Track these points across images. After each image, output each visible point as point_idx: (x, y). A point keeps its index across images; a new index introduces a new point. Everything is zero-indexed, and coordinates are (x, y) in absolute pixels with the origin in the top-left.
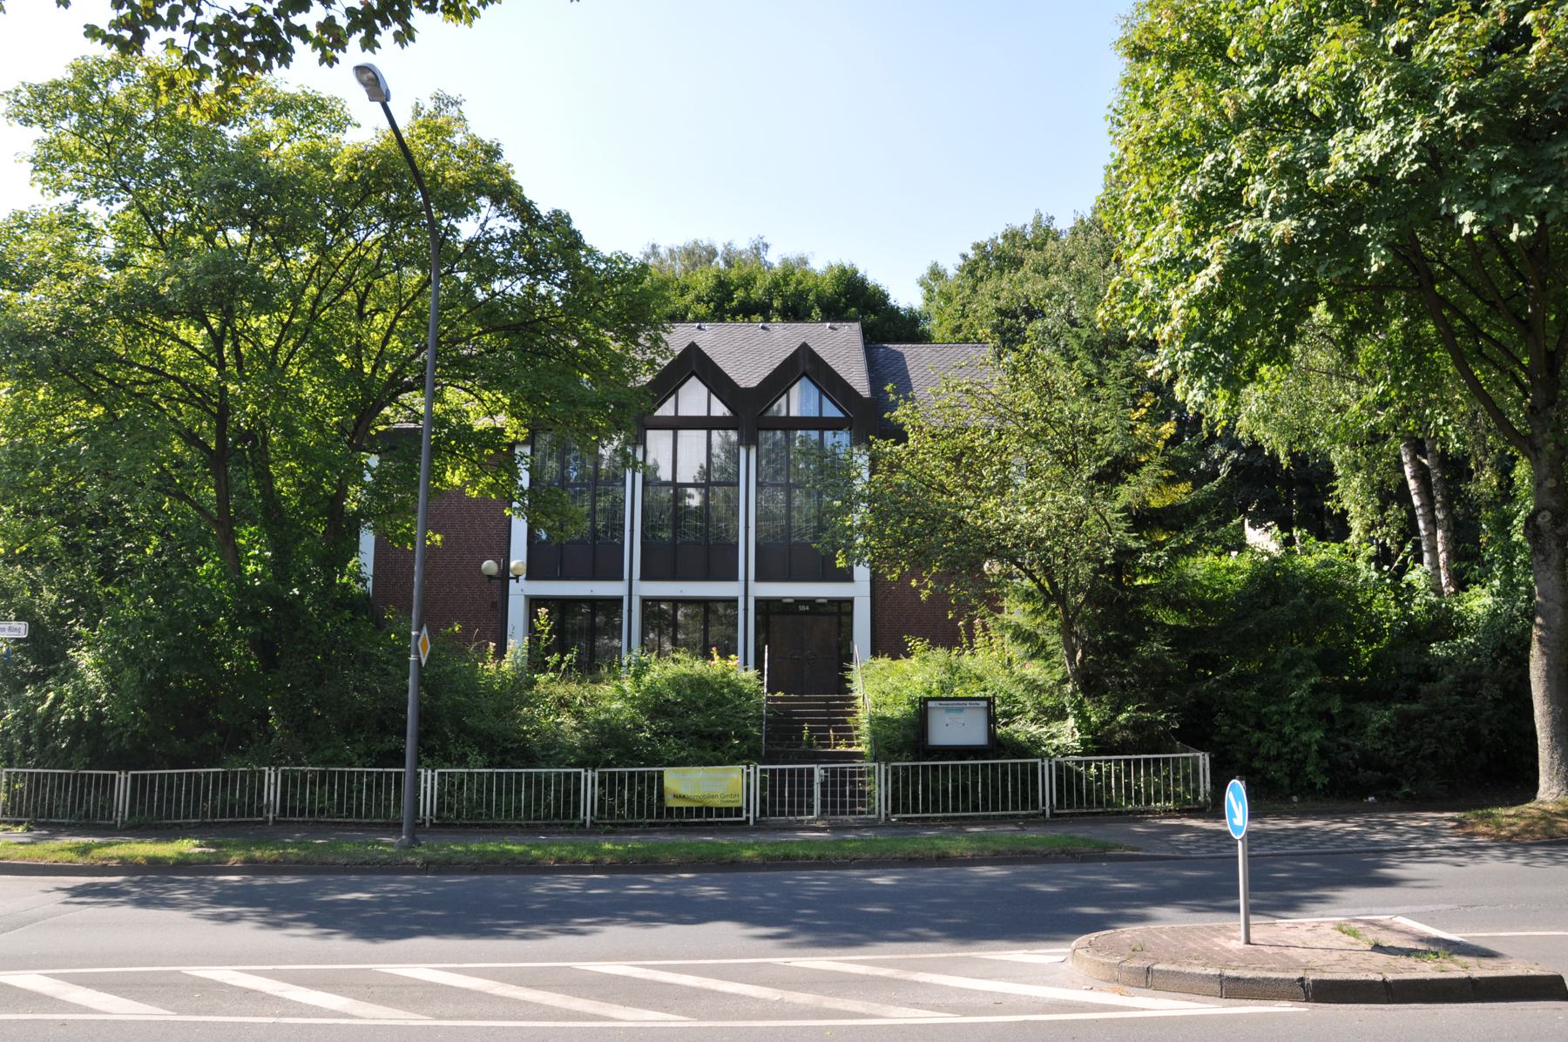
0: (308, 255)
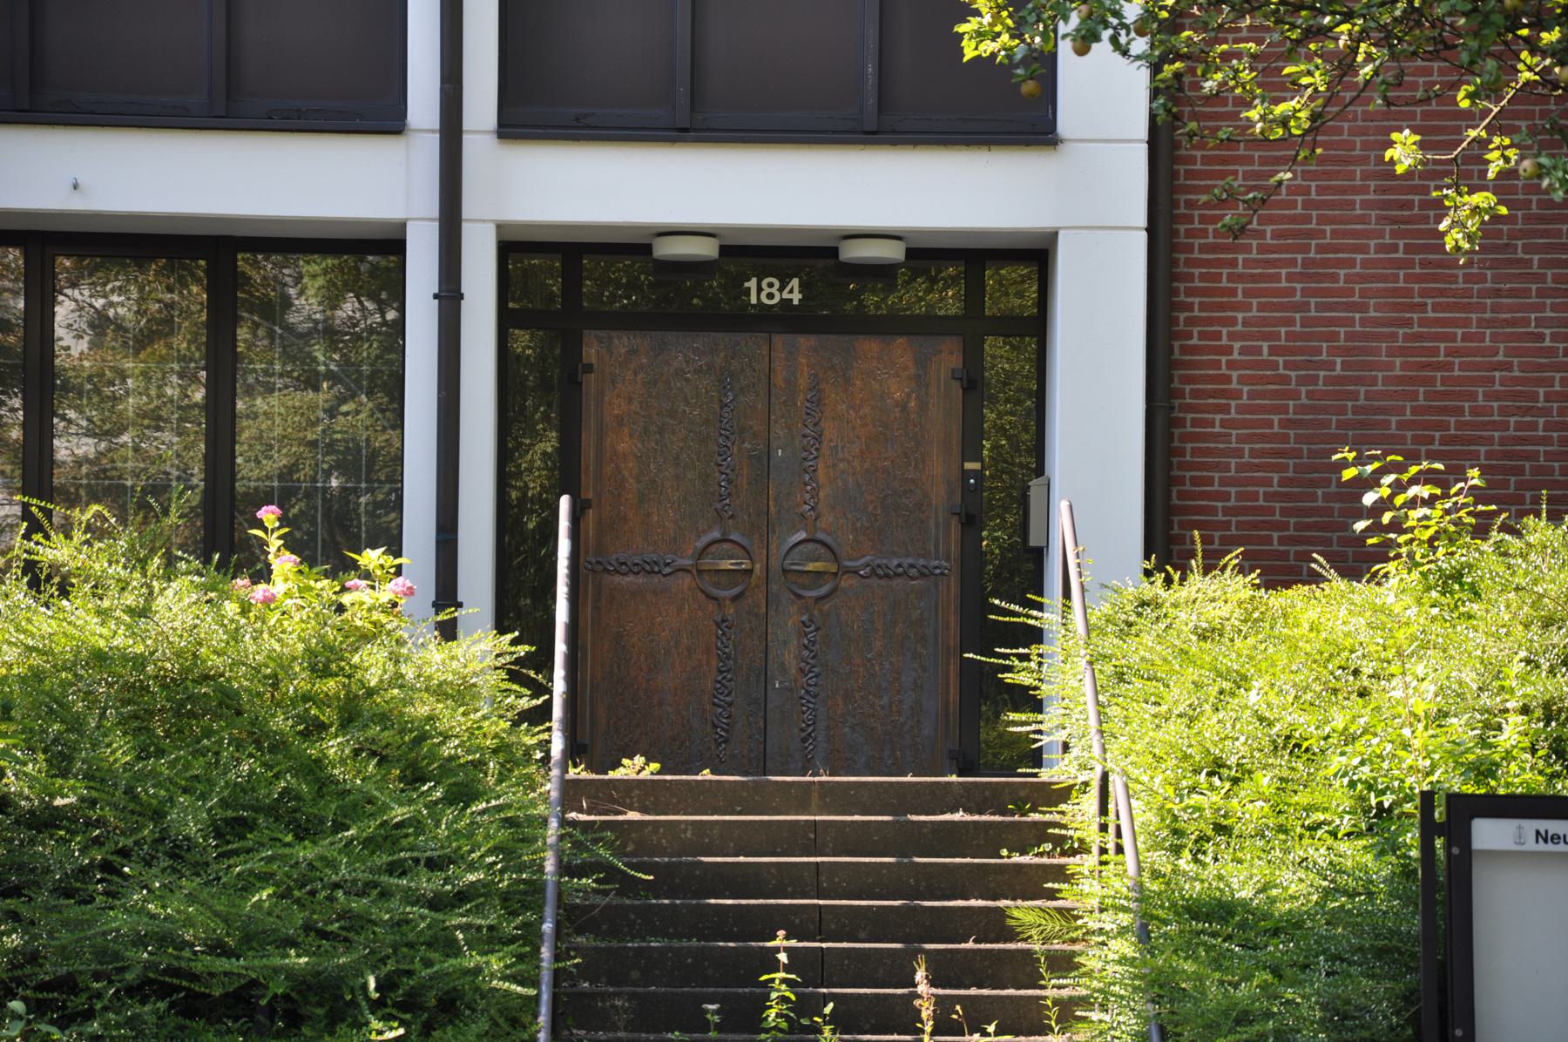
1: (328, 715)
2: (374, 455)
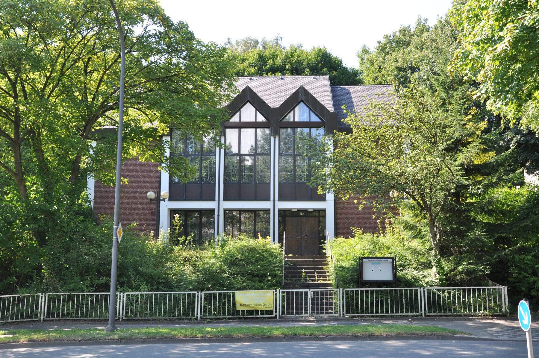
0: (58, 42)
1: (264, 251)
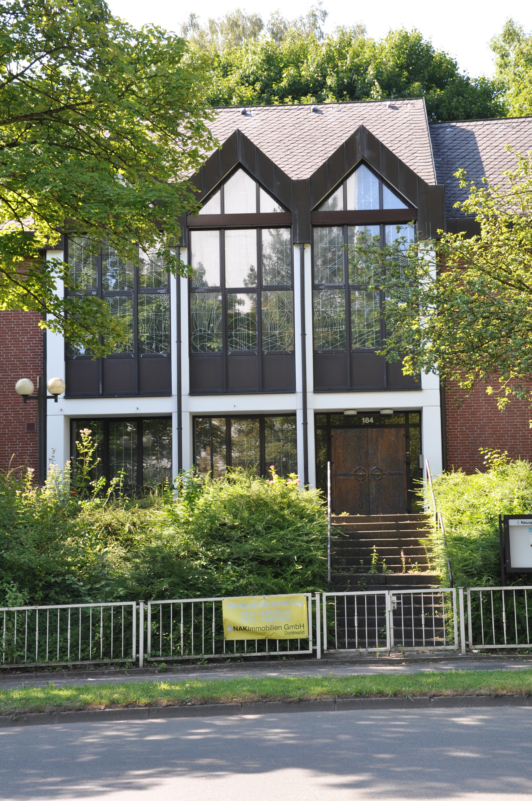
1: (285, 506)
2: (291, 454)
